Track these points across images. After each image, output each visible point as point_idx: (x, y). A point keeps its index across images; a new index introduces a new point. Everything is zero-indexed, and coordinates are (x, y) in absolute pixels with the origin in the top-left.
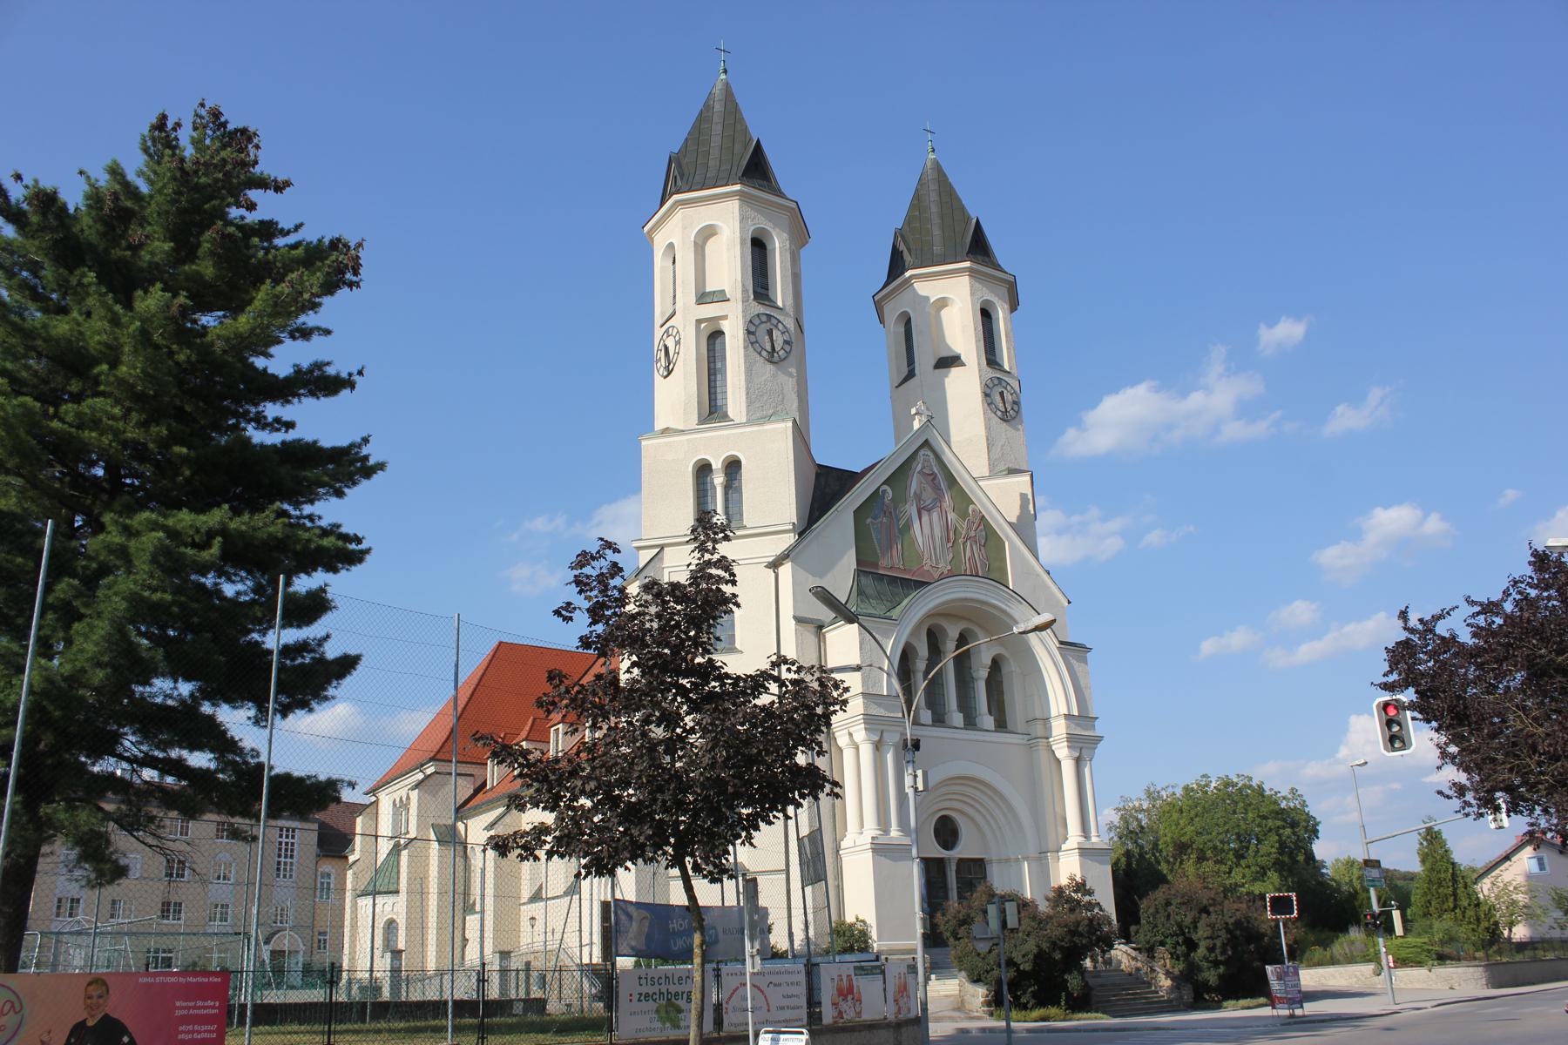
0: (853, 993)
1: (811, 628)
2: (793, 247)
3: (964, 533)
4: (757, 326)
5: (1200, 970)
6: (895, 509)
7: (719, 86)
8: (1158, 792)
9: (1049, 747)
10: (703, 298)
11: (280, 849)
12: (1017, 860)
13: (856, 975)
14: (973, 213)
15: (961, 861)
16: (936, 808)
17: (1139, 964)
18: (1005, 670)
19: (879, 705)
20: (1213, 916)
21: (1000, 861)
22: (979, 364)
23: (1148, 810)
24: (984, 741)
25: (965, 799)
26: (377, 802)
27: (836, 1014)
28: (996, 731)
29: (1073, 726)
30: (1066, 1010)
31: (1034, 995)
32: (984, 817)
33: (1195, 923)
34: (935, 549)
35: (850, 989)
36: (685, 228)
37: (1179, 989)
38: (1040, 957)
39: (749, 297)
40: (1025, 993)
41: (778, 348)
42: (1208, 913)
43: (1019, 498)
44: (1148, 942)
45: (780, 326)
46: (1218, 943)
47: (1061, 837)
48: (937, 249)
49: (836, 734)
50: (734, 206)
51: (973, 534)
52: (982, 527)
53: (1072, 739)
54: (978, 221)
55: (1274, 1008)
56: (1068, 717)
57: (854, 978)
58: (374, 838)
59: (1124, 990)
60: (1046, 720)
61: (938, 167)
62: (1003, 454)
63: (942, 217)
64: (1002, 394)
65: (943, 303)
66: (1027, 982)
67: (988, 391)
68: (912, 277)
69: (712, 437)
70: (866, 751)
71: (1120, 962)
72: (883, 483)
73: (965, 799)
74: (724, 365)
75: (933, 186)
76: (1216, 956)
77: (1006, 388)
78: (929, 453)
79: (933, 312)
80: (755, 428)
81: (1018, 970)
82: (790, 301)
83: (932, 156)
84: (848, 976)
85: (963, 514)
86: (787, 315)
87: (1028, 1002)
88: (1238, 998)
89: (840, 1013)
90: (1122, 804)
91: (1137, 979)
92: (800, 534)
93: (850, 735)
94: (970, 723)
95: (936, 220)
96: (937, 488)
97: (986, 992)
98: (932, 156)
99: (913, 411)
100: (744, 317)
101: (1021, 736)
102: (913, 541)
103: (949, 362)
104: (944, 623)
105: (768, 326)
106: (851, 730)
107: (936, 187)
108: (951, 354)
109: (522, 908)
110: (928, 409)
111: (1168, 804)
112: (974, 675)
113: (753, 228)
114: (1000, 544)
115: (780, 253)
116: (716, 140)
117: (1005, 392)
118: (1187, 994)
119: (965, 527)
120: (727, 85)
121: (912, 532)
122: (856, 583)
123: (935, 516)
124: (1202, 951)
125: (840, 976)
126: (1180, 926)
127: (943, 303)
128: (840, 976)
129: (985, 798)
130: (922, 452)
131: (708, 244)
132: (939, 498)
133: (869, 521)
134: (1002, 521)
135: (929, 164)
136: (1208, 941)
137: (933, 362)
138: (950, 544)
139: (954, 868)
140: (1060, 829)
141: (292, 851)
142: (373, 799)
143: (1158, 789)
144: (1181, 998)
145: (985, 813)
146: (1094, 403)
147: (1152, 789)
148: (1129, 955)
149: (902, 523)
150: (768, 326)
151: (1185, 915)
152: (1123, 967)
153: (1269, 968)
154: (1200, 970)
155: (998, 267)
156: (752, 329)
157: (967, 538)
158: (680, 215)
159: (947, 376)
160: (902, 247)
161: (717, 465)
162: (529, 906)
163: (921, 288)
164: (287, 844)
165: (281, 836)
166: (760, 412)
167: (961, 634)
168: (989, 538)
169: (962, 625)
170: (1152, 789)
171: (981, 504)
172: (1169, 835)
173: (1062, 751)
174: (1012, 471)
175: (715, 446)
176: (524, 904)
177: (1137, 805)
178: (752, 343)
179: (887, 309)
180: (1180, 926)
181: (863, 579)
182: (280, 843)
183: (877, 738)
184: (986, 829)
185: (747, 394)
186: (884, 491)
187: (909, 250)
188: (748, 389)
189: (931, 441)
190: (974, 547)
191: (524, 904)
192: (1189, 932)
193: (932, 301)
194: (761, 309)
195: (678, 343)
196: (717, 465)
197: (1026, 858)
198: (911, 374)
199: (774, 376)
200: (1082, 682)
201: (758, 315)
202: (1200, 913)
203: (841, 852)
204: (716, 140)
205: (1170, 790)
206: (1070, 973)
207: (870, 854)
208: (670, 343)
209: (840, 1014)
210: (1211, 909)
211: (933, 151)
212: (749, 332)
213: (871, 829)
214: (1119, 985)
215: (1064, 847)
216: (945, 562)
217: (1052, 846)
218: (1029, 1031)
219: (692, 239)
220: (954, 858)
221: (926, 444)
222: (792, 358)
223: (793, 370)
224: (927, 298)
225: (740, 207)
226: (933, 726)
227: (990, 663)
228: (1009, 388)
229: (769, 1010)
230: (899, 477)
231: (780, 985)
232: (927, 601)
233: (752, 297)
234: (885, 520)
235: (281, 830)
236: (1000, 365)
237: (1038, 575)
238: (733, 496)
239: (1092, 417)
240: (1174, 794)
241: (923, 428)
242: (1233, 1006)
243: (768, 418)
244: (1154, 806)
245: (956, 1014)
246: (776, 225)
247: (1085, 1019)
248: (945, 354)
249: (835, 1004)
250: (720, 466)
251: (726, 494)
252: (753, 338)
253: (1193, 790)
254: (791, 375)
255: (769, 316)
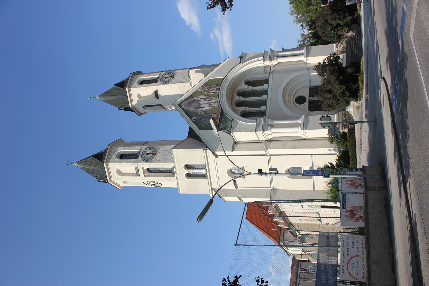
0: (353, 210)
1: (235, 146)
2: (122, 145)
3: (207, 93)
4: (145, 158)
5: (347, 22)
6: (199, 116)
7: (78, 165)
8: (292, 11)
9: (273, 66)
10: (138, 174)
11: (306, 273)
12: (310, 77)
13: (346, 208)
14: (112, 86)
15: (310, 96)
16: (293, 104)
17: (344, 41)
18: (249, 80)
19: (259, 126)
20: (328, 18)
21: (310, 82)
22: (157, 85)
23: (297, 15)
24: (272, 88)
25: (289, 99)
26: (292, 254)
27: (360, 187)
28: (268, 84)
29: (267, 59)
30: (359, 73)
31: (354, 84)
32: (296, 88)
33: (330, 25)
34: (212, 103)
35: (351, 211)
36: (118, 179)
37: (353, 29)
38: (341, 83)
39: (136, 161)
40: (353, 87)
41: (151, 152)
42: (327, 20)
43: (196, 73)
44: (337, 39)
45: (145, 151)
46: (337, 17)
47: (302, 63)
48: (124, 97)
49: (269, 138)
50: (110, 165)
51: (207, 90)
52: (205, 87)
53: (271, 60)
54: (114, 85)
55: (361, 2)
56: (264, 60)
57: (347, 209)
58: (302, 255)
59: (353, 48)
60: (265, 67)
61: (100, 96)
62: (184, 78)
63: (114, 95)
64: (165, 78)
65: (139, 96)
66: (350, 87)
67: (165, 82)
68: (132, 106)
69: (179, 173)
70: (273, 130)
71: (343, 47)
72: (191, 120)
73: (289, 99)
74: (158, 168)
75: (106, 98)
76: (342, 17)
77: (164, 76)
78: (182, 104)
79: (142, 99)
80: (175, 160)
81: (346, 90)
82: (138, 147)
83: (97, 98)
84: (346, 181)
85: (201, 93)
86: (142, 148)
87: (357, 86)
88: (357, 9)
89: (360, 185)
90: (295, 22)
91: (349, 42)
92: (207, 147)
93: (269, 135)
94: (265, 92)
95: (115, 97)
96: (193, 102)
97: (353, 101)
98: (97, 98)
99: (170, 109)
100: (142, 162)
101: (270, 75)
102: (209, 110)
103: (156, 94)
104: (235, 101)
105: (145, 155)
106: (267, 135)
107: (106, 97)
108: (154, 93)
109: (323, 223)
110: (169, 104)
111: (295, 9)
112: (251, 90)
113: (116, 159)
114: (210, 81)
115: (124, 150)
116: (93, 168)
117: (165, 77)
118: (355, 26)
119: (205, 92)
120: (78, 163)
121: (206, 110)
122: (222, 130)
123: (201, 102)
124: (341, 22)
125: (346, 184)
126: (331, 30)
127: (139, 96)
128: (346, 184)
129: (289, 88)
130: (182, 107)
131: (122, 172)
132: (196, 101)
133: (203, 125)
134: (203, 80)
135: (100, 99)
136: (337, 21)
137: (157, 99)
138: (210, 97)
139: (312, 98)
140: (300, 63)
141: (307, 269)
142: (291, 255)
143: (291, 12)
144: (356, 28)
145: (294, 87)
146: (183, 21)
147: (291, 14)
148: (341, 45)
149: (204, 114)
150: (145, 155)
151: (328, 28)
152: (345, 46)
153: (347, 4)
154: (347, 22)
155: (128, 78)
156: (146, 160)
157: (208, 91)
158: (114, 179)
159: (161, 95)
160: (124, 108)
161: (187, 172)
162: (322, 222)
163: (135, 102)
164: (305, 271)
165: (303, 272)
166: (170, 159)
167: (238, 95)
168: (208, 84)
169: (235, 95)
170: (291, 14)
171: (198, 87)
172: (304, 9)
173: (275, 62)
174: (189, 75)
175: (181, 172)
176: (322, 223)
177: (295, 18)
178: (150, 160)
179: (142, 112)
180: (331, 30)
181: (221, 128)
182: (305, 273)
183: (270, 127)
184: (300, 87)
185: (165, 162)
186: (194, 119)
187: (124, 106)
188: (164, 162)
189: (178, 104)
190: (211, 89)
191: (322, 223)
192: (334, 26)
193: (138, 99)
194: (140, 157)
195: (151, 182)
196: (187, 172)
197: (309, 74)
198: (161, 105)
199: (160, 153)
200: (253, 55)
201: (142, 158)
202: (327, 23)
203: (306, 138)
204: (93, 168)
205: (291, 8)
206: (347, 72)
207: (306, 131)
208: (152, 183)
209: (361, 218)
210: (326, 19)
211: (96, 97)
212: (147, 161)
213: (299, 129)
214: (351, 49)
215: (306, 62)
216: (216, 99)
217: (305, 66)
218: (367, 93)
219: (121, 177)
220: (309, 98)
221: (179, 105)
222: (155, 147)
223: (158, 147)
224: (138, 101)
225: (111, 162)
226: (266, 105)
227: (247, 85)
228: (164, 76)
229: (358, 256)
230: (189, 114)
231: (348, 249)
232: (227, 109)
233: (137, 160)
234: (203, 120)
235: (301, 272)
236: (157, 78)
237: (220, 68)
238: (196, 167)
239: (188, 22)
240: (292, 7)
241: (174, 106)
242: (359, 11)
243: (172, 156)
244: (296, 13)
245: (360, 110)
246: (116, 151)
247: (363, 67)
248: (154, 96)
249: (357, 187)
250: (187, 171)
251: (196, 169)
252: (149, 160)
253: (291, 2)
254: (160, 148)
255: (142, 154)
